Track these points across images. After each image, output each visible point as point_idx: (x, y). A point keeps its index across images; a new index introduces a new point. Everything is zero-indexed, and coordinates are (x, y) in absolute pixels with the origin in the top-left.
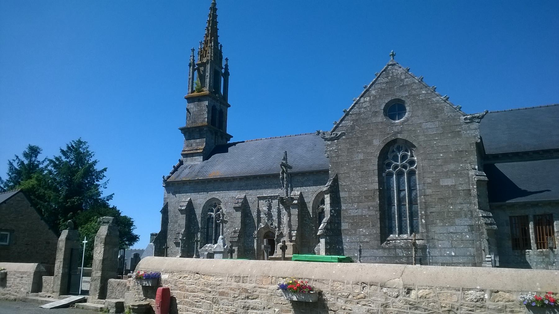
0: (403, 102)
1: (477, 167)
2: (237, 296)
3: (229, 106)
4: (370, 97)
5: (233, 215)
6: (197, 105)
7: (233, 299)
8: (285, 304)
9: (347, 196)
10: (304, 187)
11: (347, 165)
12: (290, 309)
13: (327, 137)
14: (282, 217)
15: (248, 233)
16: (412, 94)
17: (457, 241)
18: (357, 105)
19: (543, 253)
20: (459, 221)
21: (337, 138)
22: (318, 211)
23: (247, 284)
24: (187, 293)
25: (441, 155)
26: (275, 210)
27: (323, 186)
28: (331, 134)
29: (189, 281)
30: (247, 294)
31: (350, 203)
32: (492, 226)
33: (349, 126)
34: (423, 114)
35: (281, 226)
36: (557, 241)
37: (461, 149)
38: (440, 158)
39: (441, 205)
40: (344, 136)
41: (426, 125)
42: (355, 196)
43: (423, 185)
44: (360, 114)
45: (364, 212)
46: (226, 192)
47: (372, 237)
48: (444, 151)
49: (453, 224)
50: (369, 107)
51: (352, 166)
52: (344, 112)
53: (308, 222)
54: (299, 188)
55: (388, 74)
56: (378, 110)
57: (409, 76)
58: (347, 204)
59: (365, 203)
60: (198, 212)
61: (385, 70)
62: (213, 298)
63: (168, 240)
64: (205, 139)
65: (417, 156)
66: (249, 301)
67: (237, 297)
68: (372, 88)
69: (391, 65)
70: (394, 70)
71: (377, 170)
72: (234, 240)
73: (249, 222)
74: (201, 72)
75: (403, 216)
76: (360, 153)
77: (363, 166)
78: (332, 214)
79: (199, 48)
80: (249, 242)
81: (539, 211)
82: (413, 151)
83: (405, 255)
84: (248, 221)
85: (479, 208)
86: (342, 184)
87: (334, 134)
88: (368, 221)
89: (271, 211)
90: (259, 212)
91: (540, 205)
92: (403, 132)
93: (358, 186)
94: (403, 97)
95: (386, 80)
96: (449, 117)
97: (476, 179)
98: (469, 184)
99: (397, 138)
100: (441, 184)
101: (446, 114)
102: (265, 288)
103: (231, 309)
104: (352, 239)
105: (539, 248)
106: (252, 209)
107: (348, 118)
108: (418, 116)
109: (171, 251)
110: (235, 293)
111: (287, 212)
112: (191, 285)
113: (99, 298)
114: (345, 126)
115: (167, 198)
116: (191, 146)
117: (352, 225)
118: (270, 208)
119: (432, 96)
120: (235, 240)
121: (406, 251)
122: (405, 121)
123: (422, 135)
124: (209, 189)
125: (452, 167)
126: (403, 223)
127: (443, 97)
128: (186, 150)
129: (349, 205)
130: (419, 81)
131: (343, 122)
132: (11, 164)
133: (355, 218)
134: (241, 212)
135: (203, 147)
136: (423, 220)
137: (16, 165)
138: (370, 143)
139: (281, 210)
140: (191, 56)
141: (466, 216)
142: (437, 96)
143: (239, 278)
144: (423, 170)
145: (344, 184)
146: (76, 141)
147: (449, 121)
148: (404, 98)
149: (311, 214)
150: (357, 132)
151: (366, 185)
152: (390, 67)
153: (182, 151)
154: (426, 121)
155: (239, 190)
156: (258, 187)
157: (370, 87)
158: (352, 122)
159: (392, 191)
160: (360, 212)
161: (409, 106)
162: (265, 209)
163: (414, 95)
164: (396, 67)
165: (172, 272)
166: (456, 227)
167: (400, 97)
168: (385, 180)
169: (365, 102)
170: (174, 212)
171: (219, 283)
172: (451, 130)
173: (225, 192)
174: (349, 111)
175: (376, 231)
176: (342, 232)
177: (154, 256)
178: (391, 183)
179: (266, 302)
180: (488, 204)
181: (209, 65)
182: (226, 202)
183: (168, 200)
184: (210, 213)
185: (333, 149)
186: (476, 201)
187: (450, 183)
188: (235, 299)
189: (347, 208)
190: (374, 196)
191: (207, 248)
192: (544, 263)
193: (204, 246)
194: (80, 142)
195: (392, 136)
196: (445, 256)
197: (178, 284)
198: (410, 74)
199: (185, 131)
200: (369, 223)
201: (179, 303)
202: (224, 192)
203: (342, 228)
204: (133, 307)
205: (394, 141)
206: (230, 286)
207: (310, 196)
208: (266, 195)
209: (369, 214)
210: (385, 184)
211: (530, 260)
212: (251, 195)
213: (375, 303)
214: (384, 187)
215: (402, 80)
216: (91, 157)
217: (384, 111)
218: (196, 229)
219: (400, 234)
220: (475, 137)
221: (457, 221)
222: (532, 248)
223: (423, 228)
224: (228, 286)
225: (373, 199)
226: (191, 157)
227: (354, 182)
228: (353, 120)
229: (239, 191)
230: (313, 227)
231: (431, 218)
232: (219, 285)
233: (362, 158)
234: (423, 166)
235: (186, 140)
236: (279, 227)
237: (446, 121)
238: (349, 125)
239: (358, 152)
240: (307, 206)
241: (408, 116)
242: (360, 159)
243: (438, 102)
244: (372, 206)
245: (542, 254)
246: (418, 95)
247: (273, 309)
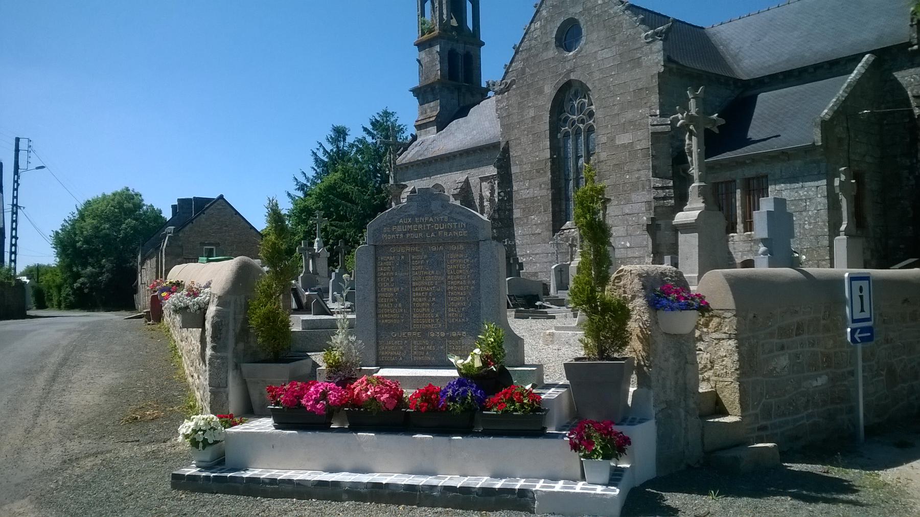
1: (658, 112)
3: (483, 44)
9: (517, 171)
17: (633, 225)
18: (527, 36)
19: (752, 238)
20: (635, 196)
32: (665, 201)
47: (544, 226)
49: (629, 202)
50: (539, 36)
56: (550, 39)
58: (518, 183)
64: (439, 101)
78: (500, 198)
81: (750, 172)
85: (654, 176)
90: (481, 198)
100: (618, 142)
104: (524, 231)
105: (749, 230)
108: (593, 42)
122: (579, 52)
123: (597, 70)
129: (521, 183)
131: (513, 64)
132: (314, 154)
135: (435, 113)
137: (320, 154)
138: (540, 92)
141: (643, 189)
146: (381, 113)
153: (416, 122)
154: (603, 48)
168: (562, 144)
173: (447, 174)
175: (548, 217)
176: (514, 222)
180: (670, 168)
187: (626, 141)
192: (752, 253)
194: (386, 114)
195: (564, 77)
199: (417, 92)
203: (514, 216)
211: (734, 249)
214: (559, 155)
216: (404, 133)
217: (556, 40)
221: (634, 197)
222: (738, 231)
225: (545, 172)
237: (624, 44)
239: (529, 106)
245: (750, 239)
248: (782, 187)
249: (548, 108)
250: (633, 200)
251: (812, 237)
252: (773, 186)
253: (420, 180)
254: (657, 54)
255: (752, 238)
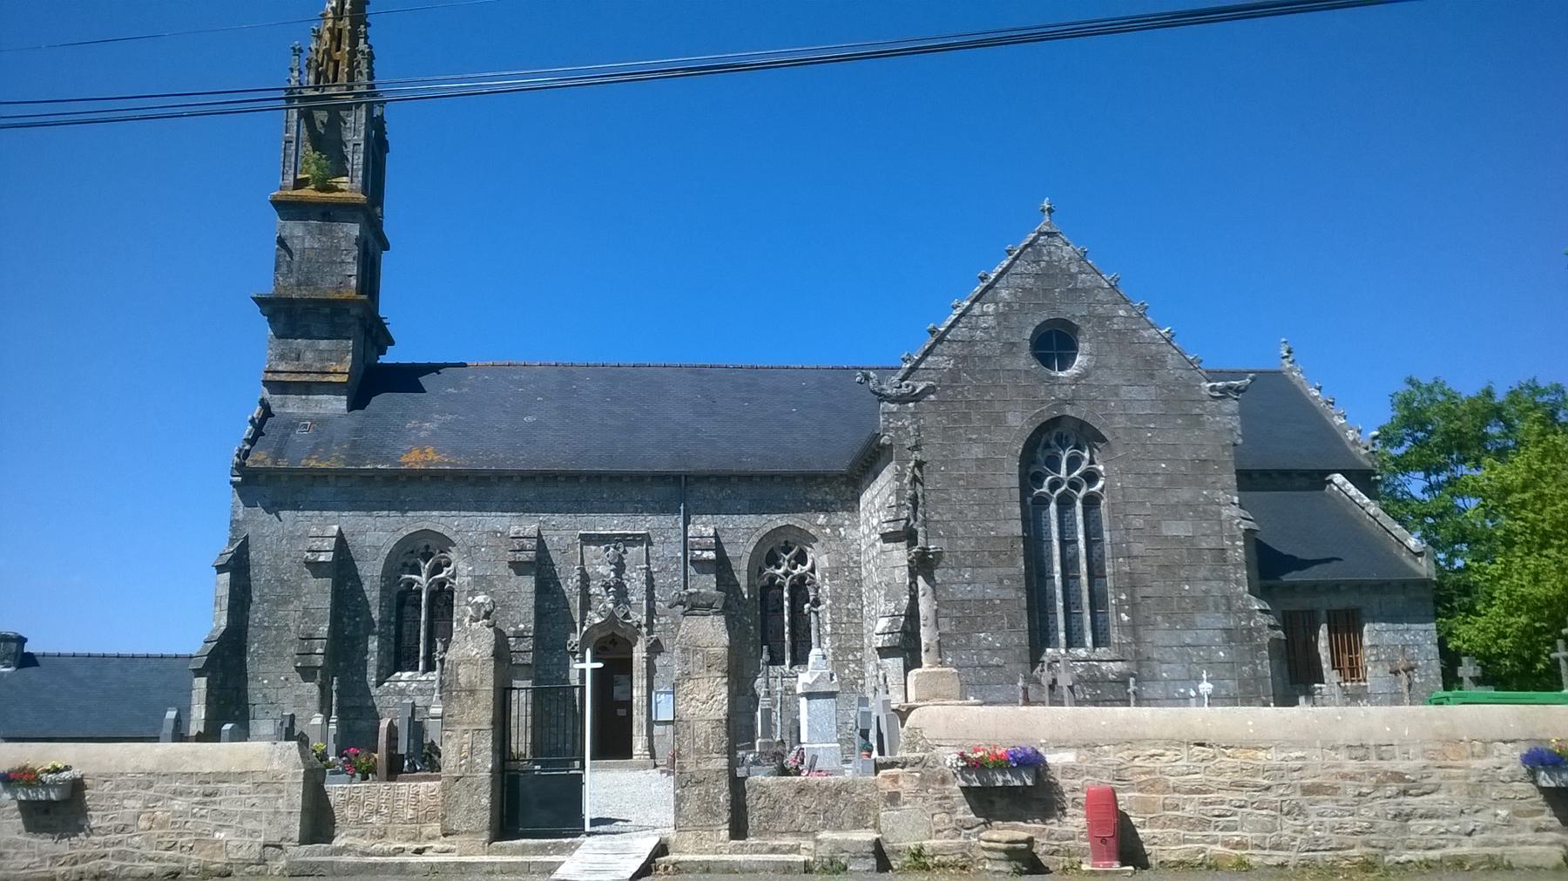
0: (1075, 329)
2: (1369, 791)
4: (997, 304)
5: (495, 586)
6: (316, 231)
7: (1357, 799)
8: (1527, 798)
10: (724, 516)
11: (943, 468)
12: (1541, 808)
13: (889, 392)
14: (656, 595)
15: (548, 639)
16: (1096, 312)
18: (963, 320)
19: (1347, 691)
21: (916, 398)
22: (759, 583)
23: (1396, 762)
24: (1177, 795)
25: (1163, 466)
26: (634, 574)
27: (777, 516)
28: (901, 387)
29: (1173, 764)
30: (1400, 784)
31: (953, 568)
33: (945, 370)
34: (1120, 365)
35: (655, 621)
36: (1370, 666)
37: (1203, 456)
38: (1160, 471)
39: (1164, 582)
40: (932, 393)
41: (1130, 392)
42: (966, 549)
43: (1124, 532)
44: (971, 342)
45: (989, 591)
46: (471, 514)
48: (1169, 456)
49: (1190, 626)
50: (994, 328)
51: (955, 473)
52: (932, 332)
53: (736, 611)
54: (709, 516)
55: (1039, 253)
57: (1089, 270)
59: (990, 570)
60: (371, 572)
61: (1030, 245)
62: (1282, 801)
63: (252, 659)
64: (351, 342)
65: (1105, 463)
66: (1409, 799)
67: (1370, 793)
68: (1001, 281)
69: (1046, 233)
70: (1053, 248)
71: (1018, 490)
72: (523, 659)
73: (552, 607)
74: (319, 125)
75: (1073, 603)
76: (975, 441)
77: (983, 476)
79: (310, 49)
80: (553, 665)
81: (1339, 602)
82: (1096, 450)
83: (1088, 697)
84: (547, 604)
86: (932, 519)
87: (907, 386)
88: (999, 613)
89: (624, 576)
90: (585, 579)
91: (1342, 588)
92: (1077, 402)
93: (972, 526)
94: (1077, 317)
95: (1033, 269)
96: (1176, 379)
97: (1241, 526)
98: (1222, 537)
99: (1064, 416)
100: (1165, 532)
101: (1172, 372)
102: (1459, 768)
103: (1355, 824)
104: (961, 658)
106: (560, 569)
107: (942, 350)
109: (264, 696)
110: (1361, 784)
111: (929, 587)
112: (1188, 774)
113: (732, 837)
114: (934, 369)
115: (244, 521)
116: (298, 359)
117: (960, 623)
118: (620, 568)
119: (1141, 326)
120: (525, 662)
121: (1090, 687)
124: (409, 501)
125: (1185, 494)
126: (1073, 620)
127: (1164, 331)
128: (280, 368)
129: (950, 571)
130: (1110, 285)
133: (966, 606)
134: (533, 578)
136: (1125, 618)
138: (998, 420)
139: (655, 576)
140: (292, 70)
141: (1217, 609)
142: (1152, 326)
143: (1359, 749)
144: (1124, 496)
145: (935, 518)
147: (1177, 388)
148: (1077, 320)
149: (745, 589)
150: (966, 388)
151: (992, 525)
152: (1042, 238)
154: (1129, 383)
155: (516, 512)
156: (579, 506)
157: (996, 280)
158: (952, 362)
159: (1047, 541)
160: (977, 591)
161: (1089, 341)
162: (606, 570)
163: (1099, 317)
164: (1058, 242)
165: (1090, 746)
166: (1198, 631)
167: (1068, 315)
169: (984, 314)
170: (276, 569)
171: (1299, 764)
172: (1182, 410)
174: (946, 331)
175: (1021, 638)
177: (1135, 706)
178: (1043, 523)
179: (1465, 797)
181: (364, 113)
182: (471, 544)
183: (249, 530)
184: (407, 576)
185: (904, 424)
186: (1242, 574)
187: (1182, 534)
188: (1362, 798)
189: (945, 579)
190: (1011, 551)
191: (404, 684)
193: (391, 678)
196: (1177, 699)
197: (1129, 773)
198: (1090, 265)
200: (1003, 619)
201: (1144, 825)
202: (462, 513)
204: (1010, 845)
205: (1056, 421)
206: (1339, 770)
207: (741, 541)
208: (609, 532)
209: (1001, 597)
210: (1032, 524)
212: (556, 528)
213: (457, 843)
215: (1073, 276)
218: (361, 626)
219: (1070, 648)
220: (1231, 430)
221: (1199, 619)
222: (1326, 681)
223: (1124, 634)
224: (1334, 770)
226: (301, 394)
227: (960, 513)
228: (955, 356)
229: (518, 514)
230: (749, 625)
231: (1144, 611)
232: (1300, 769)
233: (980, 456)
234: (1122, 488)
235: (277, 338)
236: (650, 625)
237: (1171, 388)
238: (945, 368)
239: (970, 439)
240: (733, 568)
241: (1088, 366)
242: (974, 457)
243: (1153, 342)
244: (1009, 577)
246: (1109, 318)
247: (1491, 811)
248: (1383, 627)
249: (1017, 451)
250: (1199, 625)
251: (1424, 694)
252: (1371, 625)
253: (365, 513)
254: (1230, 417)
255: (1347, 691)
